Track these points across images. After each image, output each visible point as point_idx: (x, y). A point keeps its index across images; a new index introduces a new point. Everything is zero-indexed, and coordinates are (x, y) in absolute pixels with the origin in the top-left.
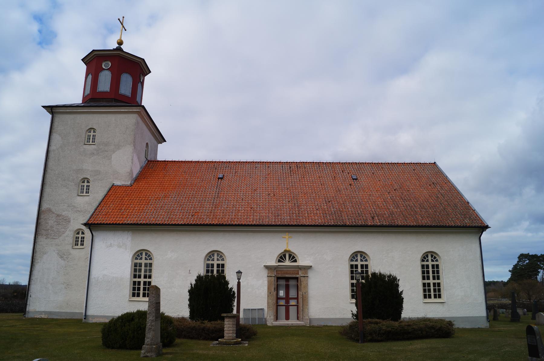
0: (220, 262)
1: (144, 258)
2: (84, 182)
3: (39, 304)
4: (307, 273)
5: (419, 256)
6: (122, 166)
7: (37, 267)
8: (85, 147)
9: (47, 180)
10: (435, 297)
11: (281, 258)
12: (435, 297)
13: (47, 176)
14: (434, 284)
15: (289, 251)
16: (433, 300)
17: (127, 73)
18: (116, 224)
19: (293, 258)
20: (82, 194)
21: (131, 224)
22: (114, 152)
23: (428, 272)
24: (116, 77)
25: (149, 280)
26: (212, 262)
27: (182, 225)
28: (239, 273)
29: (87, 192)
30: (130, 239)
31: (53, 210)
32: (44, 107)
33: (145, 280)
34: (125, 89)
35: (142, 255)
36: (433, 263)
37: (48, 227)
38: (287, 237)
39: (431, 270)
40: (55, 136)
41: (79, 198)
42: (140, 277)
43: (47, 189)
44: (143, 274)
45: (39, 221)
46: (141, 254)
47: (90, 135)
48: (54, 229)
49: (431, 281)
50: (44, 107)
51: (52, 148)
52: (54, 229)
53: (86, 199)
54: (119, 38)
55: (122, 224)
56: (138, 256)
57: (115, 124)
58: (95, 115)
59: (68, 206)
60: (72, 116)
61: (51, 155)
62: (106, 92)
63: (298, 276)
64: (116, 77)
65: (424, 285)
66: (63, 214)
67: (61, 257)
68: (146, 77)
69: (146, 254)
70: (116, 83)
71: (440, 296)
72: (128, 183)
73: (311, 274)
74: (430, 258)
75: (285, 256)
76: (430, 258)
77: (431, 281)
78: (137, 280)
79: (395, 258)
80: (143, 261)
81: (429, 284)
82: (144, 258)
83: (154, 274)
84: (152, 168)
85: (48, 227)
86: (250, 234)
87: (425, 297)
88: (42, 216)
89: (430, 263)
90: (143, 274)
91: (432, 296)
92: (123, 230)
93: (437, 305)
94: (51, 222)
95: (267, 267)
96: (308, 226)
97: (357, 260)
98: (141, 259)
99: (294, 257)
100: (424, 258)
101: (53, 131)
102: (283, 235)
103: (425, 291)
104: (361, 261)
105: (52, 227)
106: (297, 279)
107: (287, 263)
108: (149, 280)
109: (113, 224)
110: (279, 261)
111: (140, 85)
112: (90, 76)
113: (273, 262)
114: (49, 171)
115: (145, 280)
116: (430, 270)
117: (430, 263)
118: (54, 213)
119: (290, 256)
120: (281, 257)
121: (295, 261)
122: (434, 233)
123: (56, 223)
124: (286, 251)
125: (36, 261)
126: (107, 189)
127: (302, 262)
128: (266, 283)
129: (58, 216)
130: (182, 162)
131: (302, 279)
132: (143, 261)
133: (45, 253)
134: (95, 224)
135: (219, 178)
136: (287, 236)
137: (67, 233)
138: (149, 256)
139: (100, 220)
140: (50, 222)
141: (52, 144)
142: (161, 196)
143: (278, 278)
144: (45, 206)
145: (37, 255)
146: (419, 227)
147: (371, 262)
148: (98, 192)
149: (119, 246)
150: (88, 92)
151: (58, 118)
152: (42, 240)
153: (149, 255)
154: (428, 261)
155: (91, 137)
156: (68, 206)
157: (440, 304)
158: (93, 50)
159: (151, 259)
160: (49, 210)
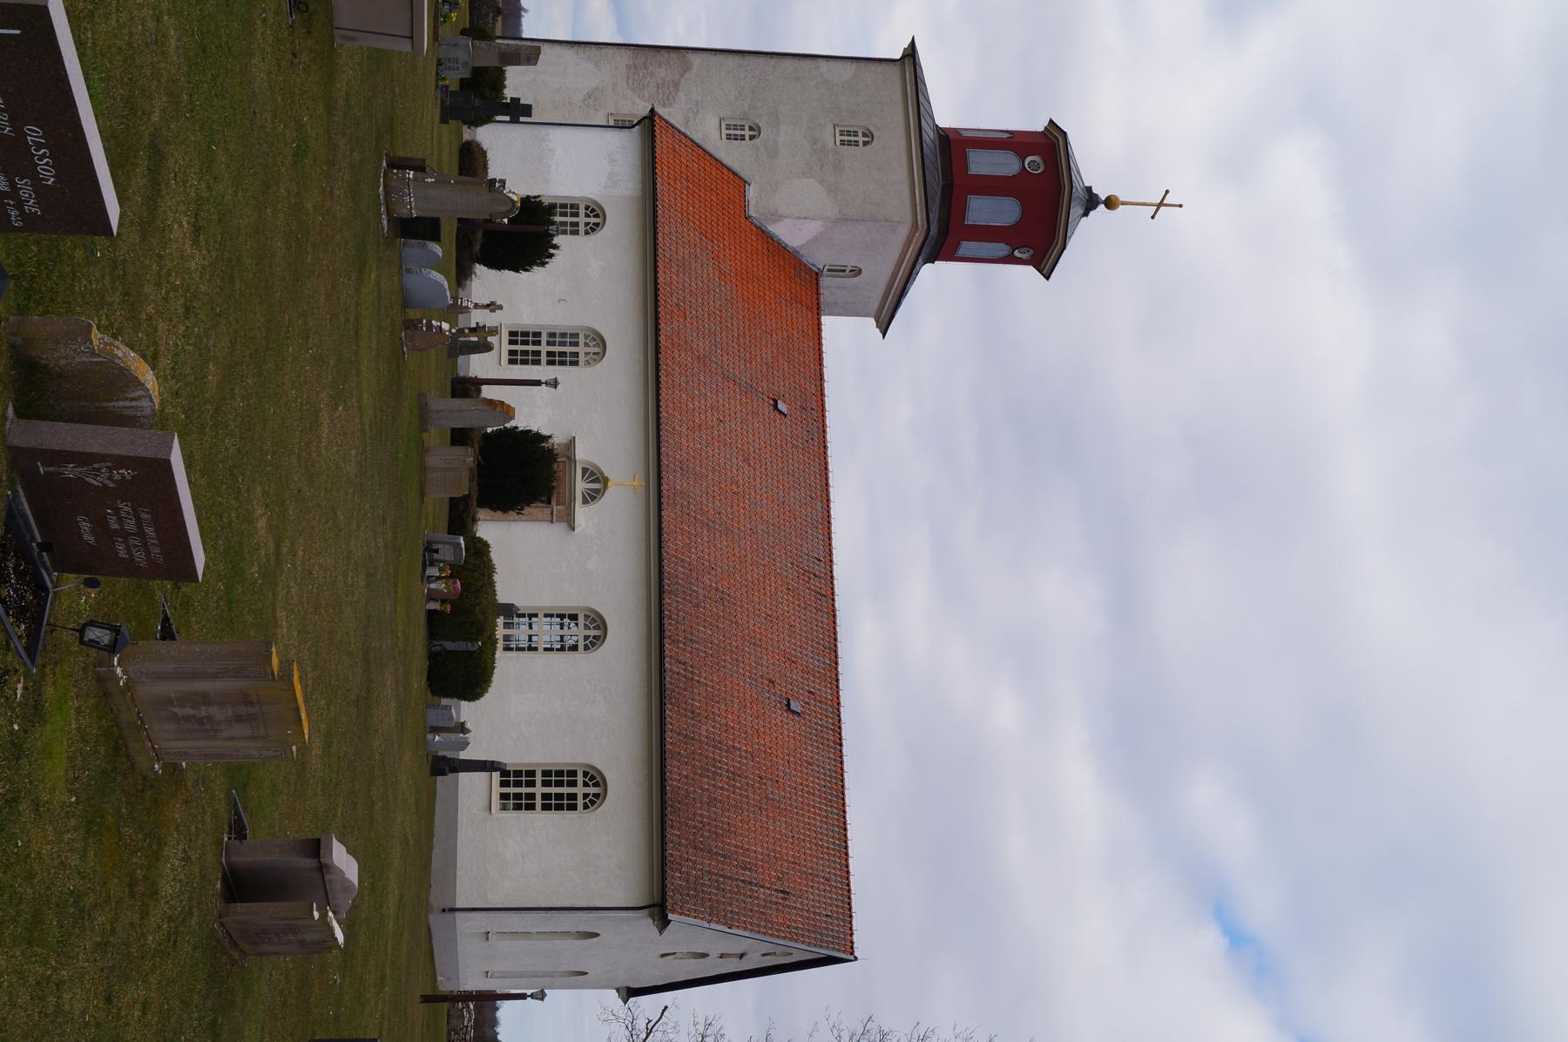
2: (751, 129)
6: (796, 211)
7: (569, 53)
8: (830, 128)
9: (747, 57)
13: (761, 59)
15: (606, 487)
18: (654, 162)
19: (591, 497)
22: (821, 182)
23: (559, 784)
24: (1009, 198)
27: (656, 278)
28: (554, 384)
29: (729, 137)
30: (627, 193)
32: (913, 43)
36: (580, 797)
39: (565, 790)
40: (851, 68)
43: (731, 61)
46: (596, 785)
47: (858, 137)
49: (539, 790)
50: (913, 43)
51: (822, 64)
55: (654, 173)
56: (592, 778)
57: (891, 189)
58: (903, 142)
60: (898, 97)
62: (966, 167)
63: (554, 502)
64: (1009, 198)
66: (681, 94)
67: (589, 95)
68: (1031, 268)
69: (596, 796)
70: (993, 186)
72: (752, 212)
73: (558, 529)
74: (592, 790)
75: (596, 481)
76: (592, 790)
77: (539, 790)
81: (532, 784)
84: (800, 289)
86: (642, 413)
87: (512, 334)
88: (674, 55)
89: (580, 790)
91: (506, 790)
92: (643, 182)
93: (485, 795)
96: (660, 516)
97: (586, 784)
99: (593, 498)
100: (595, 778)
101: (862, 64)
102: (640, 475)
104: (587, 224)
105: (652, 74)
109: (654, 157)
110: (585, 470)
111: (1002, 249)
113: (581, 454)
114: (773, 62)
116: (559, 789)
117: (580, 790)
119: (597, 491)
120: (593, 473)
121: (585, 501)
124: (606, 480)
125: (580, 49)
126: (735, 166)
127: (582, 513)
129: (676, 85)
130: (820, 344)
133: (597, 65)
136: (639, 482)
138: (593, 803)
139: (662, 140)
140: (663, 71)
141: (832, 63)
142: (740, 317)
144: (695, 59)
145: (593, 51)
146: (663, 752)
148: (732, 155)
149: (611, 176)
150: (980, 164)
151: (894, 73)
152: (624, 57)
153: (592, 802)
154: (586, 784)
159: (586, 807)
160: (687, 68)
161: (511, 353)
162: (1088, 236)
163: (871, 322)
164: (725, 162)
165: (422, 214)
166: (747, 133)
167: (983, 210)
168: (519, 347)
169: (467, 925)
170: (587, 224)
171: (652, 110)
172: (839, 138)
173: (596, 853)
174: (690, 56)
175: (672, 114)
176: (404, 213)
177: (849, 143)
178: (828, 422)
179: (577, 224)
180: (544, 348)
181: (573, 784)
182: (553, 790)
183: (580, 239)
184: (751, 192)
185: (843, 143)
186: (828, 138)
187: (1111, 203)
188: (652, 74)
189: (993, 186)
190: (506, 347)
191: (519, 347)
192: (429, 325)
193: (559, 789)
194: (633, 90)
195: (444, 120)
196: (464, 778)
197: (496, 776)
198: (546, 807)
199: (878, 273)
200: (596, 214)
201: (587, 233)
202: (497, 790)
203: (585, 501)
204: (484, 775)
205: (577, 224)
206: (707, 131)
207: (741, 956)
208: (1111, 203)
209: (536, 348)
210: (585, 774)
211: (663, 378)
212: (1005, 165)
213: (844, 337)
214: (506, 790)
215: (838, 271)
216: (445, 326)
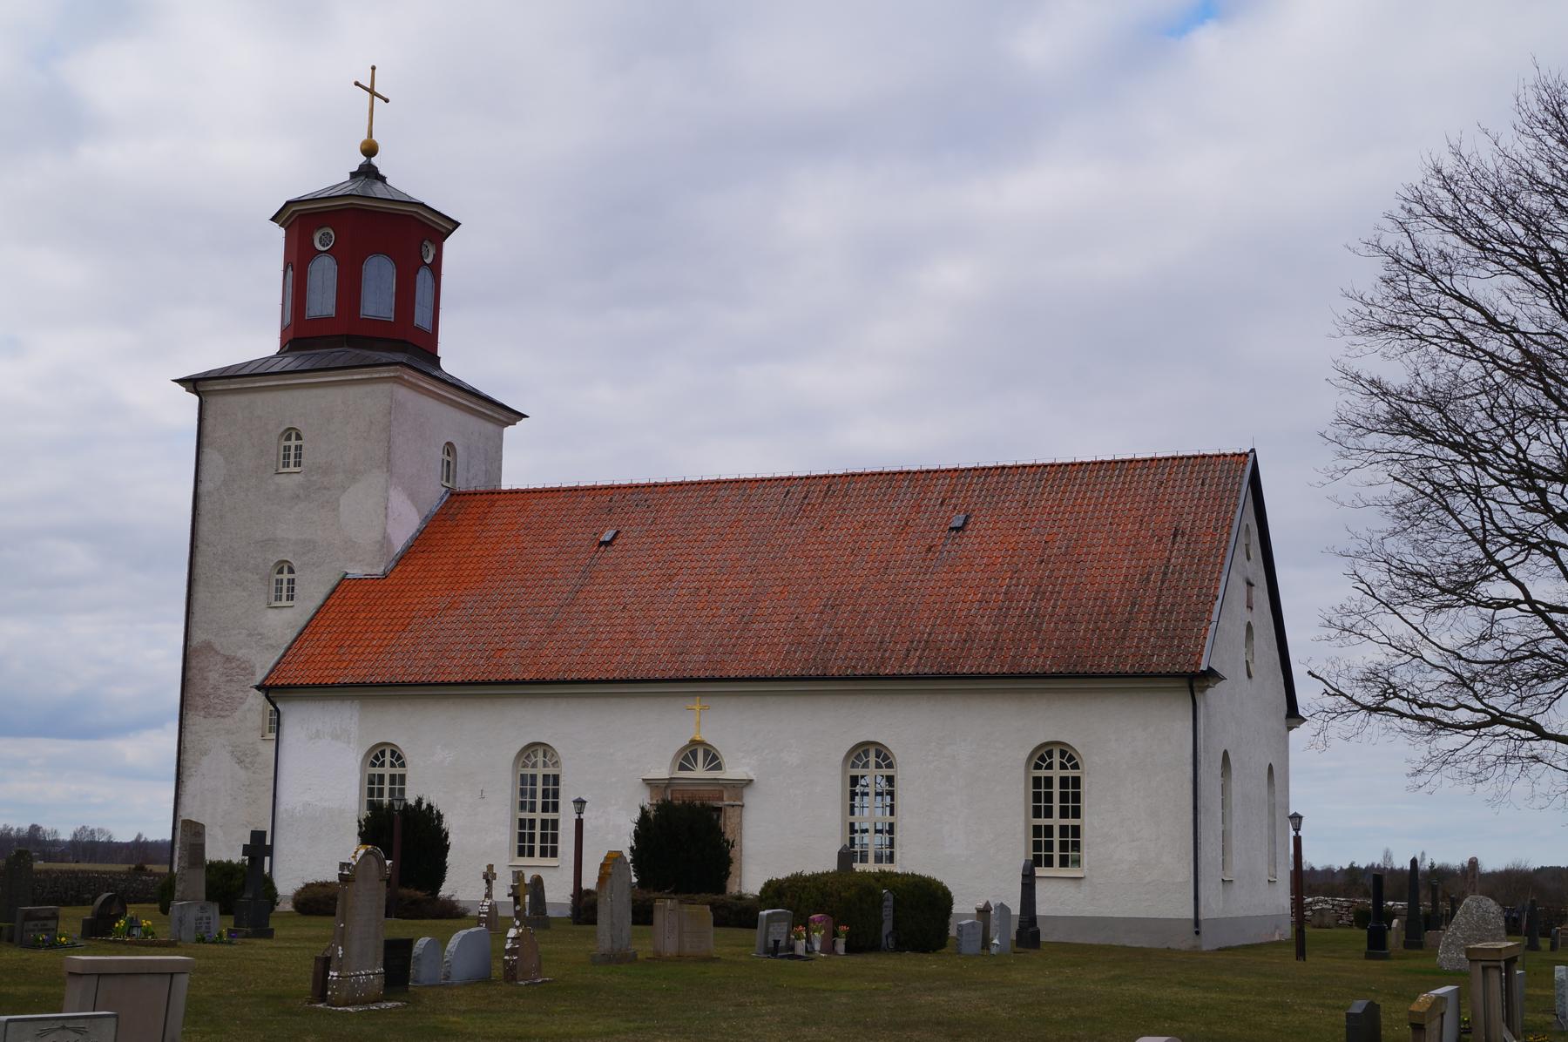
0: (550, 771)
1: (387, 763)
2: (281, 572)
4: (741, 798)
6: (376, 519)
7: (190, 786)
8: (281, 479)
11: (692, 752)
14: (1064, 829)
15: (701, 743)
17: (376, 252)
19: (714, 760)
20: (278, 604)
21: (351, 685)
22: (344, 489)
24: (364, 264)
25: (1075, 822)
26: (1048, 773)
27: (456, 684)
31: (218, 648)
32: (179, 381)
33: (1065, 822)
34: (378, 302)
35: (1051, 756)
36: (1065, 773)
37: (209, 689)
38: (697, 708)
41: (271, 613)
43: (201, 594)
45: (189, 675)
46: (866, 753)
48: (221, 692)
49: (1056, 821)
51: (205, 487)
52: (221, 692)
53: (287, 615)
54: (365, 137)
56: (1042, 758)
58: (297, 393)
59: (250, 635)
60: (244, 399)
61: (205, 505)
63: (720, 804)
64: (364, 264)
66: (239, 654)
67: (240, 762)
68: (449, 245)
69: (393, 753)
70: (349, 289)
71: (1077, 862)
72: (379, 570)
73: (750, 798)
77: (539, 816)
83: (1086, 804)
85: (209, 689)
87: (521, 853)
89: (1056, 774)
91: (1056, 860)
92: (342, 698)
93: (1063, 885)
94: (214, 676)
95: (649, 783)
99: (715, 758)
100: (1042, 756)
101: (205, 441)
105: (216, 688)
108: (1075, 822)
110: (682, 768)
111: (424, 277)
112: (290, 273)
113: (663, 772)
114: (202, 546)
115: (1065, 822)
117: (1056, 774)
118: (217, 653)
119: (706, 753)
120: (686, 758)
121: (719, 767)
122: (1005, 691)
123: (224, 679)
124: (694, 743)
126: (335, 582)
127: (733, 770)
129: (228, 659)
130: (535, 491)
131: (730, 811)
133: (204, 753)
134: (277, 687)
135: (602, 543)
136: (696, 704)
142: (500, 586)
144: (198, 637)
145: (189, 757)
149: (336, 737)
151: (215, 403)
152: (194, 719)
153: (1070, 758)
155: (292, 452)
156: (250, 635)
157: (1070, 882)
158: (288, 203)
159: (1076, 766)
160: (208, 647)
161: (543, 854)
162: (410, 176)
163: (508, 431)
164: (319, 602)
165: (380, 961)
166: (286, 576)
167: (378, 302)
169: (1213, 907)
171: (258, 688)
173: (1130, 754)
175: (263, 664)
176: (378, 982)
177: (298, 456)
180: (539, 816)
181: (1049, 781)
182: (1056, 805)
183: (411, 773)
184: (356, 571)
186: (290, 481)
187: (370, 150)
188: (216, 688)
189: (349, 289)
190: (537, 860)
191: (537, 845)
192: (512, 952)
193: (1056, 792)
194: (234, 710)
195: (269, 934)
196: (1041, 910)
198: (1077, 813)
199: (451, 423)
200: (381, 754)
201: (403, 765)
202: (1056, 871)
203: (719, 767)
204: (1039, 886)
206: (283, 623)
207: (1250, 584)
208: (370, 150)
211: (574, 676)
212: (324, 273)
213: (524, 464)
214: (1056, 860)
215: (449, 469)
216: (512, 933)
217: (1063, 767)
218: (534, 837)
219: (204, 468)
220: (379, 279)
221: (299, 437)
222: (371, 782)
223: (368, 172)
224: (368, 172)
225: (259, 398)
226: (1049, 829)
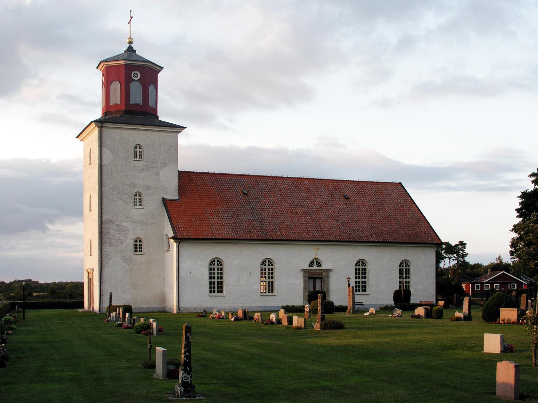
1: (216, 264)
3: (93, 302)
5: (260, 261)
10: (218, 292)
11: (311, 264)
12: (218, 292)
13: (103, 189)
15: (317, 259)
16: (216, 294)
22: (161, 169)
25: (221, 280)
33: (218, 280)
37: (111, 236)
40: (104, 150)
42: (214, 278)
43: (105, 202)
44: (216, 276)
51: (104, 162)
58: (140, 132)
65: (210, 283)
66: (123, 224)
69: (218, 261)
70: (126, 93)
71: (222, 292)
73: (331, 274)
75: (313, 262)
77: (216, 280)
78: (212, 280)
79: (339, 263)
80: (404, 268)
81: (359, 282)
82: (216, 264)
83: (367, 275)
85: (111, 236)
86: (291, 246)
87: (210, 292)
90: (216, 276)
91: (216, 291)
98: (359, 266)
99: (319, 263)
100: (212, 263)
103: (210, 287)
104: (362, 266)
105: (114, 236)
106: (321, 278)
107: (315, 267)
108: (221, 280)
110: (310, 266)
112: (104, 88)
113: (307, 267)
115: (218, 280)
117: (267, 267)
119: (317, 262)
120: (311, 263)
121: (320, 266)
122: (223, 243)
127: (324, 267)
128: (302, 281)
129: (118, 226)
131: (325, 278)
132: (361, 267)
136: (287, 247)
137: (128, 241)
140: (112, 231)
143: (309, 278)
144: (105, 217)
145: (104, 260)
147: (368, 267)
150: (116, 99)
151: (106, 131)
153: (220, 262)
154: (359, 266)
159: (272, 265)
160: (111, 221)
167: (136, 98)
168: (361, 288)
170: (362, 266)
172: (138, 159)
174: (103, 220)
177: (140, 155)
178: (224, 173)
179: (406, 269)
180: (361, 280)
185: (140, 158)
186: (138, 163)
187: (131, 43)
188: (114, 236)
191: (361, 288)
197: (356, 293)
202: (361, 293)
203: (320, 266)
204: (355, 296)
205: (406, 269)
208: (131, 43)
209: (361, 283)
210: (211, 265)
212: (116, 87)
214: (216, 291)
217: (269, 265)
218: (360, 286)
219: (103, 155)
220: (136, 89)
221: (140, 148)
222: (262, 270)
223: (130, 50)
224: (130, 50)
225: (125, 132)
226: (214, 282)
